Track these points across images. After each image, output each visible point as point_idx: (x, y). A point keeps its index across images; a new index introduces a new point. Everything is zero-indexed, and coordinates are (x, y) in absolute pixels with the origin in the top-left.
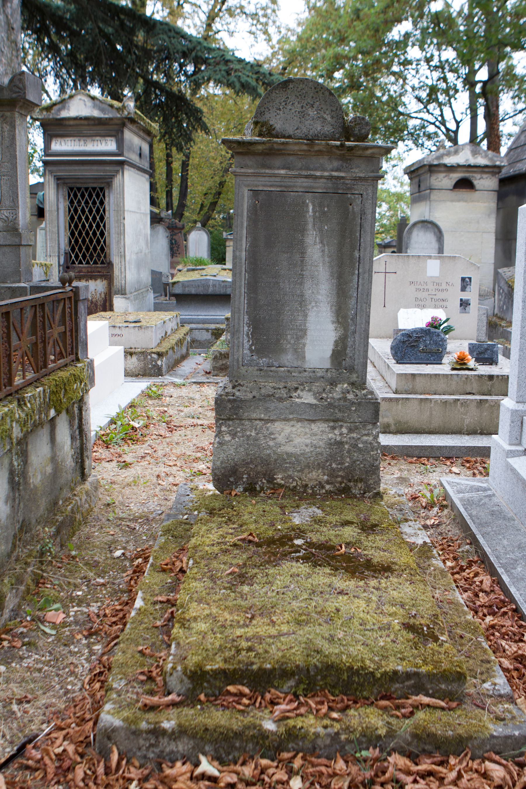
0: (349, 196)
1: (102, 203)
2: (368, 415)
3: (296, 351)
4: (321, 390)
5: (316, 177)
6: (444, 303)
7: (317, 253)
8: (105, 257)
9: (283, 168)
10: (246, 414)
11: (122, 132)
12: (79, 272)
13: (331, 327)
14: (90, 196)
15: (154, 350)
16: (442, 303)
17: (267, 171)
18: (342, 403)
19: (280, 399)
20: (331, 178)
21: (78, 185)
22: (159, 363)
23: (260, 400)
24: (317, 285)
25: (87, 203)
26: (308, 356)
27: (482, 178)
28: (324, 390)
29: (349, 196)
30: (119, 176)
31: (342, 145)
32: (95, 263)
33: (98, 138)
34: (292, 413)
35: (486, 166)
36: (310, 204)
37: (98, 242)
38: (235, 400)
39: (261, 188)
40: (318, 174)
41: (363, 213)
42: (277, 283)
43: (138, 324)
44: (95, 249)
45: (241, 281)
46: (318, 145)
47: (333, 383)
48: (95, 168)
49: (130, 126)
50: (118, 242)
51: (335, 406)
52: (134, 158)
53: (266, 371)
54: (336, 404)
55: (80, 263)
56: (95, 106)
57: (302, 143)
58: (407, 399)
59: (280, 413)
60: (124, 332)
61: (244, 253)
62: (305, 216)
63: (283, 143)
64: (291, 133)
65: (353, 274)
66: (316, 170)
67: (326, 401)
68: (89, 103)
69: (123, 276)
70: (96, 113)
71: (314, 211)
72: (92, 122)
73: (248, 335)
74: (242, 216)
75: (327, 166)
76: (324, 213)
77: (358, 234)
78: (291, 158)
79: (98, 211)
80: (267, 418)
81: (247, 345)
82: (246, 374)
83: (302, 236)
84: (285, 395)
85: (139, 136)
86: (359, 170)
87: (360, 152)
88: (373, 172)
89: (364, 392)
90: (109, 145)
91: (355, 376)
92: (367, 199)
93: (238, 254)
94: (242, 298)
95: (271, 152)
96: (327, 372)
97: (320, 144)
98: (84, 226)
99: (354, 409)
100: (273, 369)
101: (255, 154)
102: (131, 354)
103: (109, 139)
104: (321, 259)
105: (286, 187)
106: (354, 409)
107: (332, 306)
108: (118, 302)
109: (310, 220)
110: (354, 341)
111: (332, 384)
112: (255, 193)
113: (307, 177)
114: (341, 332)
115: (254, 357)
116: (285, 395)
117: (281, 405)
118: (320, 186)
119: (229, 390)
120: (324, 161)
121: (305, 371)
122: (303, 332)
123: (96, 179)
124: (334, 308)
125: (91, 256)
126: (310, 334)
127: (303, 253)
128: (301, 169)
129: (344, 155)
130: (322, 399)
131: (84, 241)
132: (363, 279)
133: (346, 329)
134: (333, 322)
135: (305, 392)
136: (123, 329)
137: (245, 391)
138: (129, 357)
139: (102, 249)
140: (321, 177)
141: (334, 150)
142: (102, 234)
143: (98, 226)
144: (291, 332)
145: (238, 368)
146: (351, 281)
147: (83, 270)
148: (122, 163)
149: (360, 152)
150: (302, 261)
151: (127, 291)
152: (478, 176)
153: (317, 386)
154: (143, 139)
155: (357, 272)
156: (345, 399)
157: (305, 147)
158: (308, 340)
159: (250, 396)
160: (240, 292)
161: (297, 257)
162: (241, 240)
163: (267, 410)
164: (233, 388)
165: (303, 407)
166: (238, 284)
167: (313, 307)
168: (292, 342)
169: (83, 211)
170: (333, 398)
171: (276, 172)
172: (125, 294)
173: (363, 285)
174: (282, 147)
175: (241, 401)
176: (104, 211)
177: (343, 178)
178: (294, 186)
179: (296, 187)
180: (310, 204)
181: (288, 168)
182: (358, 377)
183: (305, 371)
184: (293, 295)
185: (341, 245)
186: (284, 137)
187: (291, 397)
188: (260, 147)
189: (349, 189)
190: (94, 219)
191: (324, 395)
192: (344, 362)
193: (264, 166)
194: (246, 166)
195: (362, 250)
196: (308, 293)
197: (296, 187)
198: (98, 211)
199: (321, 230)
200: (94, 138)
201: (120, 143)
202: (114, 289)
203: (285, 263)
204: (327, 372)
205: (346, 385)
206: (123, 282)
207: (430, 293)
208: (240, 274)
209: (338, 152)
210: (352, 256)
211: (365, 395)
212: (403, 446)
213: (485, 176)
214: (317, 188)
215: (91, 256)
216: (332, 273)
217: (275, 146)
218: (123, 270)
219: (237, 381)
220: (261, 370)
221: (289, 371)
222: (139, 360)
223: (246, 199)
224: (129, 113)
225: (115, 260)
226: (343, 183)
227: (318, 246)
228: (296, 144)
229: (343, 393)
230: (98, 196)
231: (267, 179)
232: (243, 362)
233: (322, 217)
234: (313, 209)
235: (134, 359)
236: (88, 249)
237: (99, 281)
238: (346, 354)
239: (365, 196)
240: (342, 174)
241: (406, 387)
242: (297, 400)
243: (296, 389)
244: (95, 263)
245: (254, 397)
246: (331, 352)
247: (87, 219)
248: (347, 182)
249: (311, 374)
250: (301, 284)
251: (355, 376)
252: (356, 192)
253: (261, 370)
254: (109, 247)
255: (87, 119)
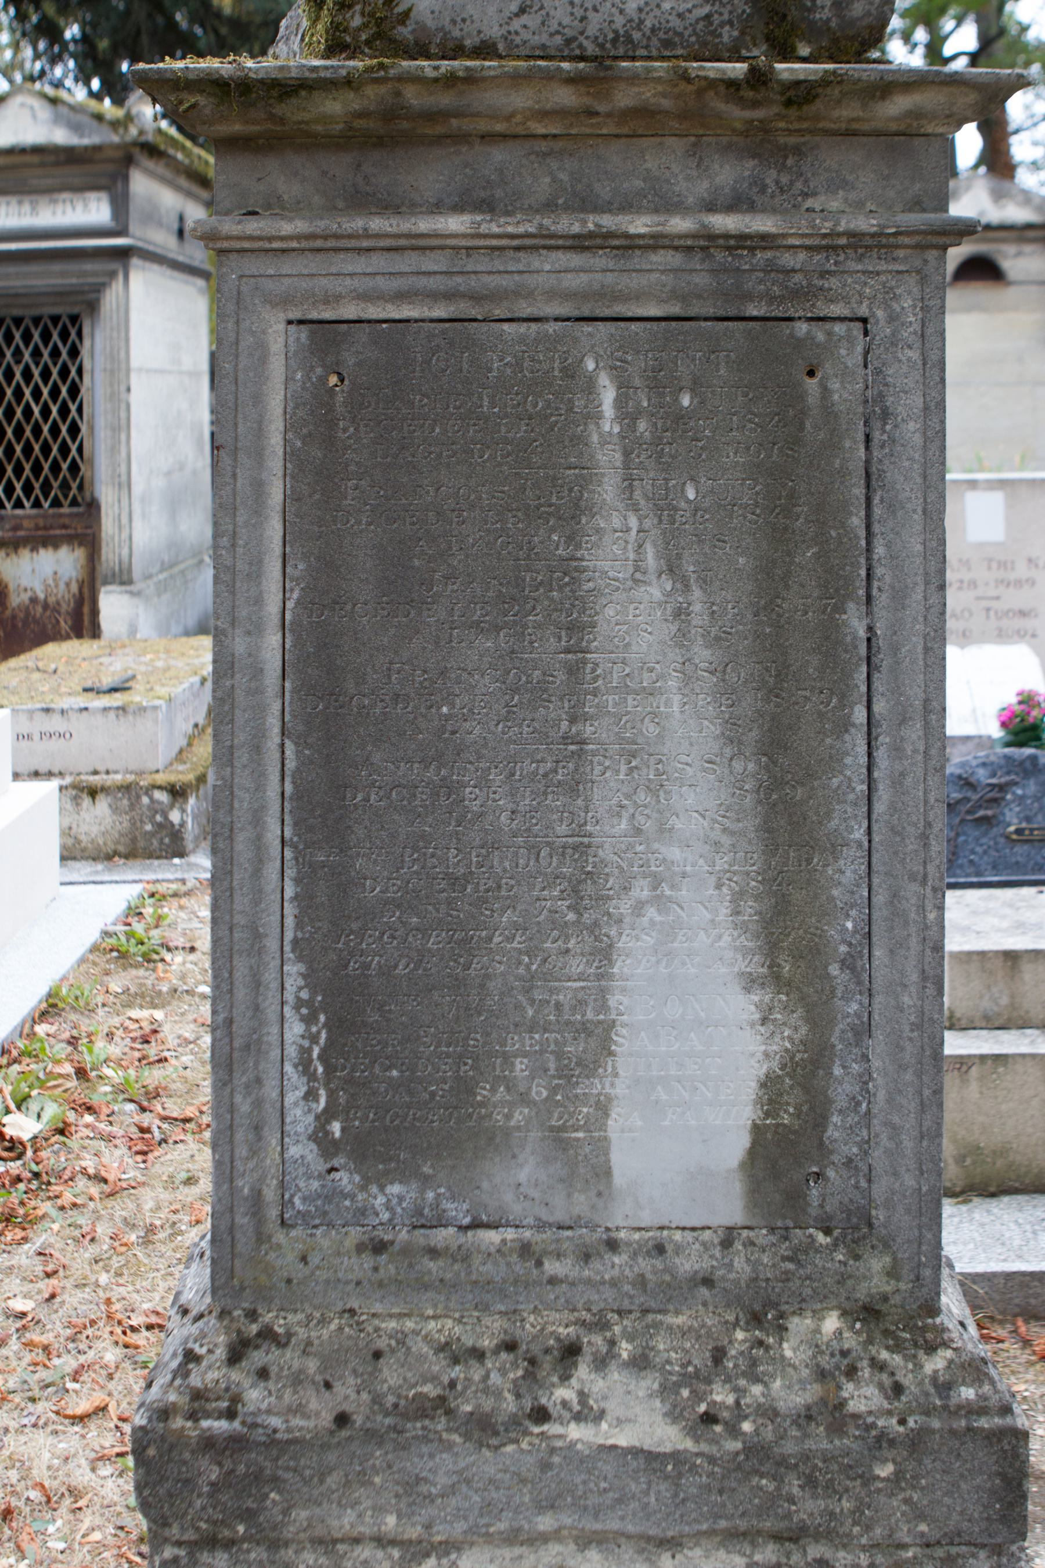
0: (802, 328)
1: (74, 353)
2: (965, 1502)
3: (558, 1140)
4: (701, 1359)
5: (629, 245)
6: (1028, 624)
7: (650, 625)
8: (81, 488)
9: (458, 208)
10: (301, 1515)
11: (126, 179)
12: (15, 528)
13: (743, 1007)
14: (46, 337)
15: (161, 778)
16: (1019, 623)
17: (377, 224)
18: (819, 1440)
19: (484, 1429)
20: (706, 243)
21: (17, 312)
22: (175, 816)
23: (372, 1436)
24: (655, 789)
25: (37, 354)
26: (624, 1163)
27: (1018, 254)
28: (719, 1355)
29: (802, 328)
30: (117, 286)
31: (758, 78)
32: (56, 503)
33: (65, 195)
34: (551, 1506)
35: (1029, 226)
36: (604, 380)
37: (64, 450)
38: (236, 1443)
39: (350, 311)
40: (639, 225)
41: (877, 412)
42: (451, 788)
43: (117, 700)
44: (55, 468)
45: (260, 787)
46: (633, 79)
47: (764, 1312)
48: (57, 267)
49: (150, 164)
50: (114, 450)
51: (782, 1462)
52: (163, 240)
53: (407, 1251)
54: (789, 1448)
55: (19, 504)
56: (57, 120)
57: (549, 77)
58: (1000, 1059)
59: (488, 1508)
60: (77, 724)
61: (273, 639)
62: (580, 441)
63: (451, 80)
64: (494, 31)
65: (845, 725)
66: (627, 206)
67: (733, 1430)
68: (44, 111)
69: (125, 535)
70: (61, 136)
71: (627, 415)
72: (52, 158)
73: (304, 1065)
74: (259, 455)
75: (681, 186)
76: (680, 417)
77: (857, 521)
78: (498, 154)
79: (64, 373)
80: (414, 1532)
81: (301, 1119)
82: (300, 1272)
83: (572, 539)
84: (509, 1404)
85: (178, 188)
86: (849, 202)
87: (848, 112)
88: (917, 205)
89: (936, 1363)
90: (93, 211)
91: (877, 1264)
92: (894, 342)
93: (239, 645)
94: (272, 870)
95: (391, 133)
96: (727, 1243)
97: (646, 81)
98: (28, 412)
99: (885, 1471)
100: (443, 1236)
101: (306, 141)
102: (93, 793)
103: (92, 196)
104: (675, 655)
105: (476, 298)
106: (885, 1471)
107: (738, 897)
108: (113, 606)
109: (608, 460)
110: (865, 1078)
111: (756, 1319)
112: (324, 335)
113: (580, 243)
114: (792, 1030)
115: (344, 1179)
116: (509, 1404)
117: (487, 1464)
118: (651, 286)
119: (209, 1375)
120: (665, 161)
121: (613, 1245)
122: (592, 1041)
123: (61, 295)
124: (749, 908)
125: (46, 488)
126: (635, 1051)
127: (577, 630)
128: (549, 206)
129: (764, 128)
130: (709, 1418)
131: (28, 450)
132: (897, 750)
133: (817, 1014)
134: (750, 983)
135: (615, 1375)
136: (73, 716)
137: (297, 1380)
138: (86, 801)
139: (74, 468)
140: (656, 242)
141: (718, 104)
142: (74, 430)
143: (64, 411)
144: (531, 1041)
145: (261, 1238)
146: (834, 761)
147: (26, 523)
148: (123, 254)
149: (848, 112)
150: (574, 671)
151: (136, 574)
152: (1011, 249)
153: (679, 1335)
154: (189, 194)
155: (860, 715)
156: (833, 1414)
157: (565, 97)
158: (622, 1081)
159: (321, 1410)
160: (258, 843)
161: (548, 649)
162: (256, 574)
163: (412, 1491)
164: (235, 1357)
165: (608, 1468)
166: (243, 802)
167: (639, 907)
168: (539, 1092)
169: (27, 375)
170: (768, 1412)
171: (424, 225)
172: (130, 582)
173: (897, 781)
174: (445, 100)
175: (273, 1443)
176: (80, 372)
177: (765, 241)
178: (516, 293)
179: (529, 295)
180: (604, 380)
181: (487, 206)
182: (893, 1273)
183: (613, 1245)
184: (534, 850)
185: (771, 580)
186: (457, 51)
187: (541, 1415)
188: (334, 107)
189: (797, 294)
190: (55, 393)
191: (722, 1396)
192: (814, 1193)
193: (361, 200)
194: (274, 205)
195: (882, 600)
196: (611, 834)
197: (529, 295)
198: (64, 373)
199: (664, 507)
200: (56, 196)
201: (120, 205)
202: (103, 568)
203: (487, 684)
204: (727, 1243)
205: (831, 1323)
206: (125, 552)
207: (980, 591)
208: (257, 749)
209: (737, 114)
210: (830, 634)
211: (944, 1388)
212: (1009, 1276)
213: (1028, 248)
214: (638, 297)
215: (46, 488)
216: (731, 723)
217: (414, 97)
218: (125, 520)
219: (252, 1315)
220: (379, 1247)
221: (525, 1249)
222: (115, 809)
223: (277, 367)
224: (141, 132)
225: (106, 495)
226: (770, 268)
227: (655, 591)
228: (517, 79)
229: (822, 1375)
230: (64, 335)
231: (378, 262)
232: (285, 1204)
233: (666, 441)
234: (620, 403)
235: (102, 806)
236: (37, 469)
237: (64, 552)
238: (823, 1150)
239: (881, 328)
240: (762, 224)
241: (986, 1004)
242: (575, 1432)
243: (571, 1351)
244: (56, 503)
245: (342, 1419)
246: (742, 1141)
247: (37, 394)
248: (788, 260)
249: (644, 1265)
250: (575, 787)
251: (877, 1264)
252: (837, 309)
253: (379, 1247)
254: (91, 463)
255: (37, 150)
